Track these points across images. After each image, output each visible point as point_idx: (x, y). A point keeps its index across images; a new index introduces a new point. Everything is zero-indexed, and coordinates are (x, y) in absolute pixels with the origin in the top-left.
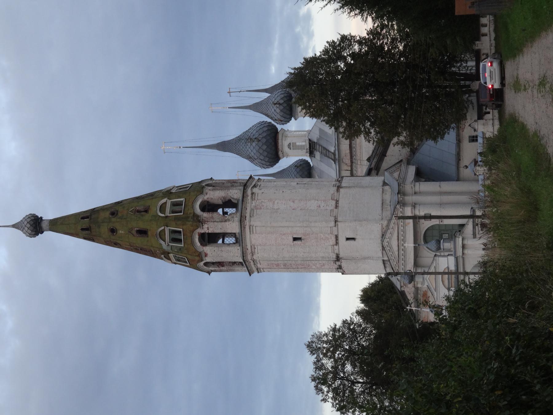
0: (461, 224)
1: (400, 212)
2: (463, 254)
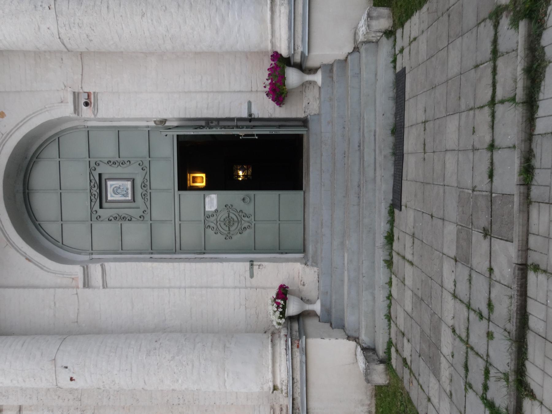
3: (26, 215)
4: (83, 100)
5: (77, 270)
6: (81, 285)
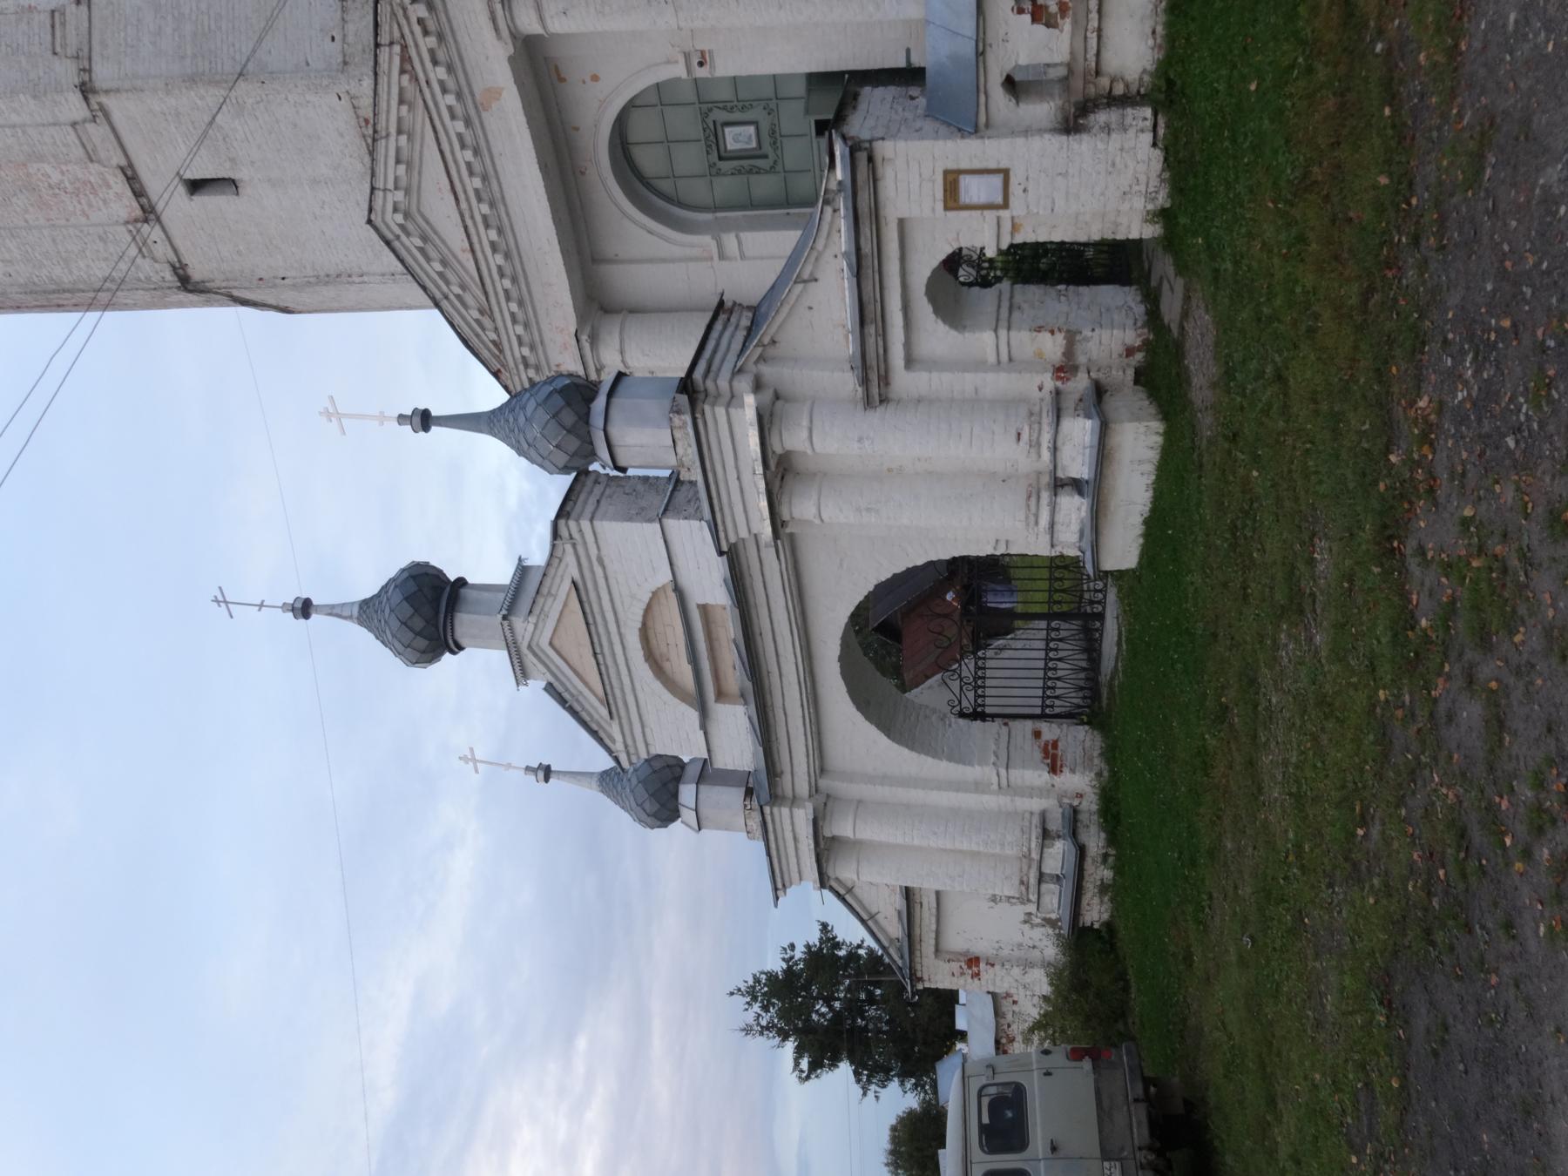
0: (822, 69)
1: (417, 29)
2: (777, 523)
3: (630, 173)
4: (695, 61)
5: (707, 240)
6: (716, 257)
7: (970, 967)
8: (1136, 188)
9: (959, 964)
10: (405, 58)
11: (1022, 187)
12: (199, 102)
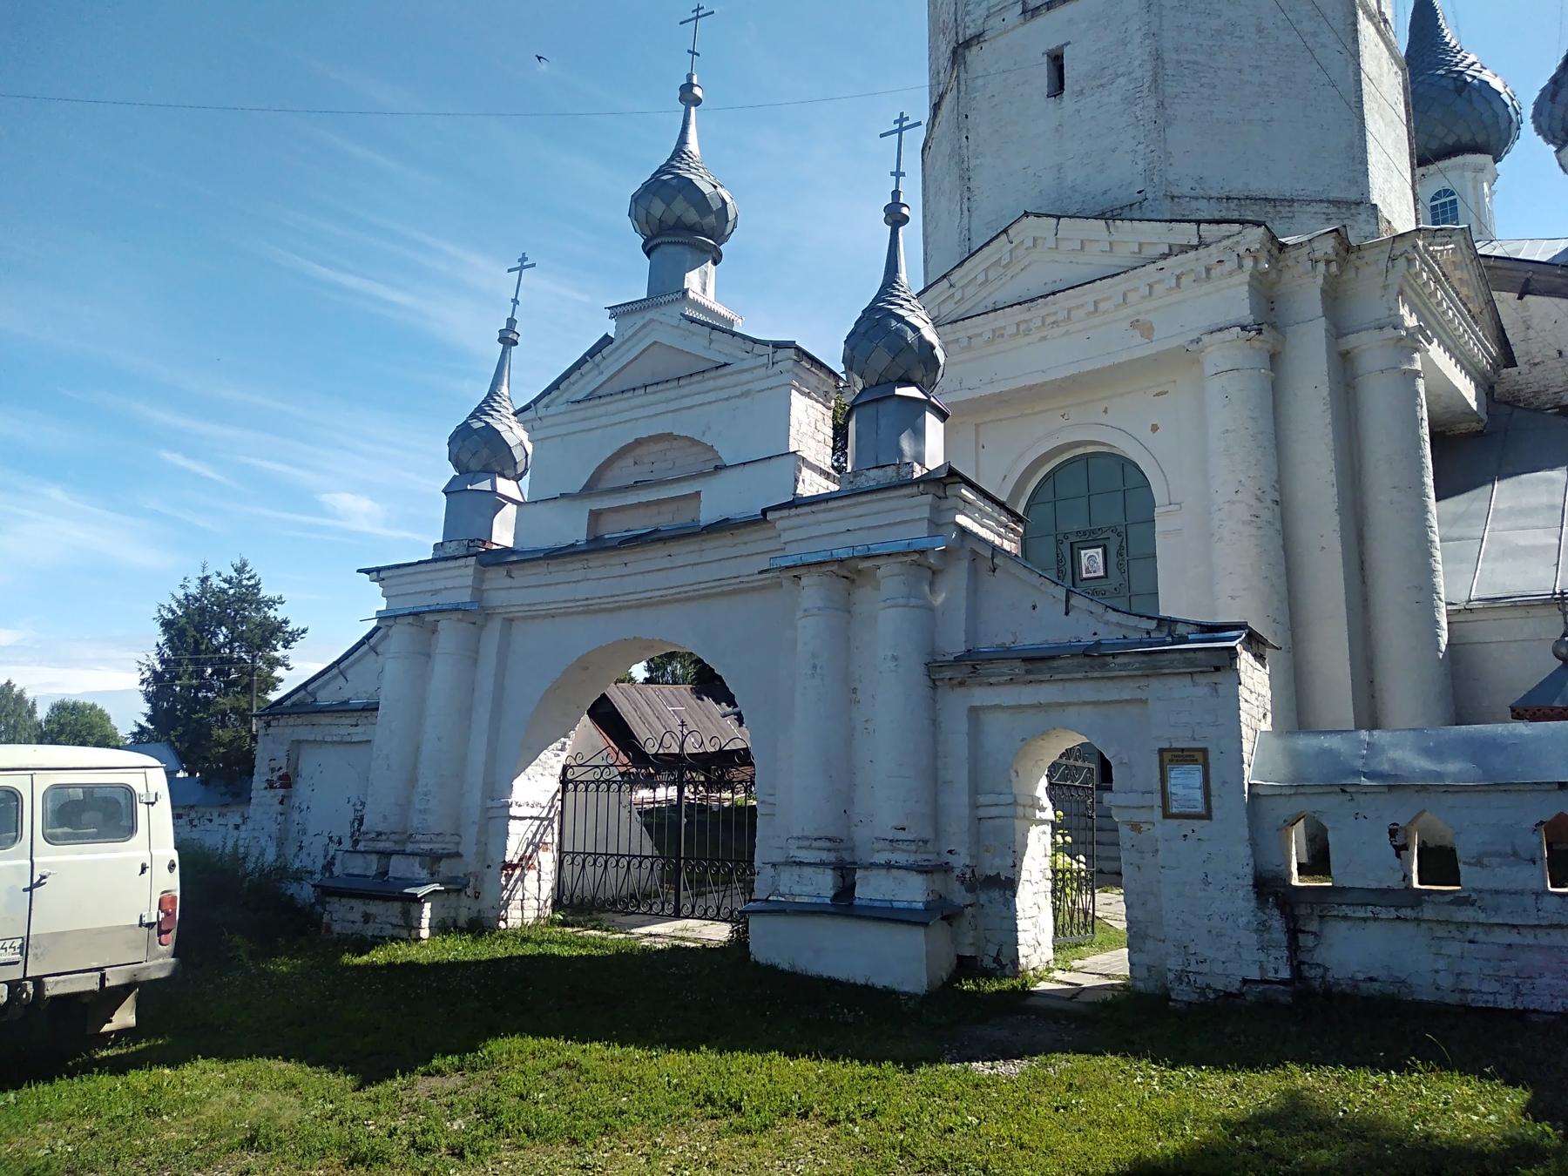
7: (280, 778)
8: (1193, 962)
9: (284, 766)
10: (1185, 249)
11: (1189, 833)
12: (1137, 63)
